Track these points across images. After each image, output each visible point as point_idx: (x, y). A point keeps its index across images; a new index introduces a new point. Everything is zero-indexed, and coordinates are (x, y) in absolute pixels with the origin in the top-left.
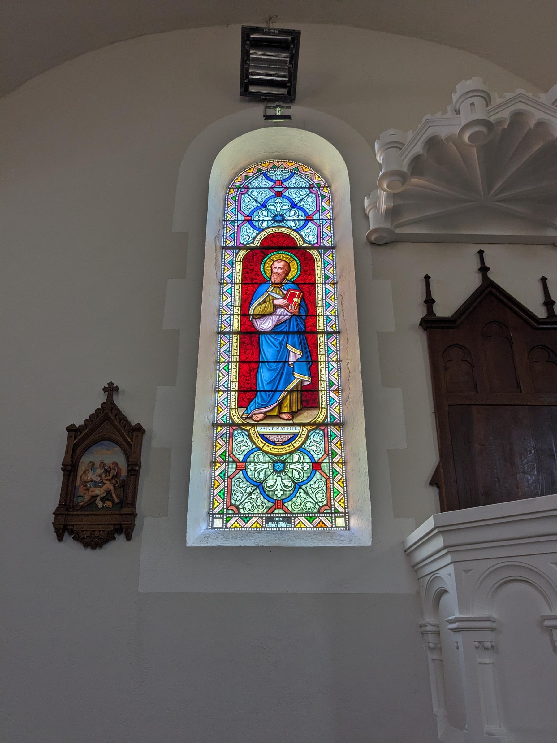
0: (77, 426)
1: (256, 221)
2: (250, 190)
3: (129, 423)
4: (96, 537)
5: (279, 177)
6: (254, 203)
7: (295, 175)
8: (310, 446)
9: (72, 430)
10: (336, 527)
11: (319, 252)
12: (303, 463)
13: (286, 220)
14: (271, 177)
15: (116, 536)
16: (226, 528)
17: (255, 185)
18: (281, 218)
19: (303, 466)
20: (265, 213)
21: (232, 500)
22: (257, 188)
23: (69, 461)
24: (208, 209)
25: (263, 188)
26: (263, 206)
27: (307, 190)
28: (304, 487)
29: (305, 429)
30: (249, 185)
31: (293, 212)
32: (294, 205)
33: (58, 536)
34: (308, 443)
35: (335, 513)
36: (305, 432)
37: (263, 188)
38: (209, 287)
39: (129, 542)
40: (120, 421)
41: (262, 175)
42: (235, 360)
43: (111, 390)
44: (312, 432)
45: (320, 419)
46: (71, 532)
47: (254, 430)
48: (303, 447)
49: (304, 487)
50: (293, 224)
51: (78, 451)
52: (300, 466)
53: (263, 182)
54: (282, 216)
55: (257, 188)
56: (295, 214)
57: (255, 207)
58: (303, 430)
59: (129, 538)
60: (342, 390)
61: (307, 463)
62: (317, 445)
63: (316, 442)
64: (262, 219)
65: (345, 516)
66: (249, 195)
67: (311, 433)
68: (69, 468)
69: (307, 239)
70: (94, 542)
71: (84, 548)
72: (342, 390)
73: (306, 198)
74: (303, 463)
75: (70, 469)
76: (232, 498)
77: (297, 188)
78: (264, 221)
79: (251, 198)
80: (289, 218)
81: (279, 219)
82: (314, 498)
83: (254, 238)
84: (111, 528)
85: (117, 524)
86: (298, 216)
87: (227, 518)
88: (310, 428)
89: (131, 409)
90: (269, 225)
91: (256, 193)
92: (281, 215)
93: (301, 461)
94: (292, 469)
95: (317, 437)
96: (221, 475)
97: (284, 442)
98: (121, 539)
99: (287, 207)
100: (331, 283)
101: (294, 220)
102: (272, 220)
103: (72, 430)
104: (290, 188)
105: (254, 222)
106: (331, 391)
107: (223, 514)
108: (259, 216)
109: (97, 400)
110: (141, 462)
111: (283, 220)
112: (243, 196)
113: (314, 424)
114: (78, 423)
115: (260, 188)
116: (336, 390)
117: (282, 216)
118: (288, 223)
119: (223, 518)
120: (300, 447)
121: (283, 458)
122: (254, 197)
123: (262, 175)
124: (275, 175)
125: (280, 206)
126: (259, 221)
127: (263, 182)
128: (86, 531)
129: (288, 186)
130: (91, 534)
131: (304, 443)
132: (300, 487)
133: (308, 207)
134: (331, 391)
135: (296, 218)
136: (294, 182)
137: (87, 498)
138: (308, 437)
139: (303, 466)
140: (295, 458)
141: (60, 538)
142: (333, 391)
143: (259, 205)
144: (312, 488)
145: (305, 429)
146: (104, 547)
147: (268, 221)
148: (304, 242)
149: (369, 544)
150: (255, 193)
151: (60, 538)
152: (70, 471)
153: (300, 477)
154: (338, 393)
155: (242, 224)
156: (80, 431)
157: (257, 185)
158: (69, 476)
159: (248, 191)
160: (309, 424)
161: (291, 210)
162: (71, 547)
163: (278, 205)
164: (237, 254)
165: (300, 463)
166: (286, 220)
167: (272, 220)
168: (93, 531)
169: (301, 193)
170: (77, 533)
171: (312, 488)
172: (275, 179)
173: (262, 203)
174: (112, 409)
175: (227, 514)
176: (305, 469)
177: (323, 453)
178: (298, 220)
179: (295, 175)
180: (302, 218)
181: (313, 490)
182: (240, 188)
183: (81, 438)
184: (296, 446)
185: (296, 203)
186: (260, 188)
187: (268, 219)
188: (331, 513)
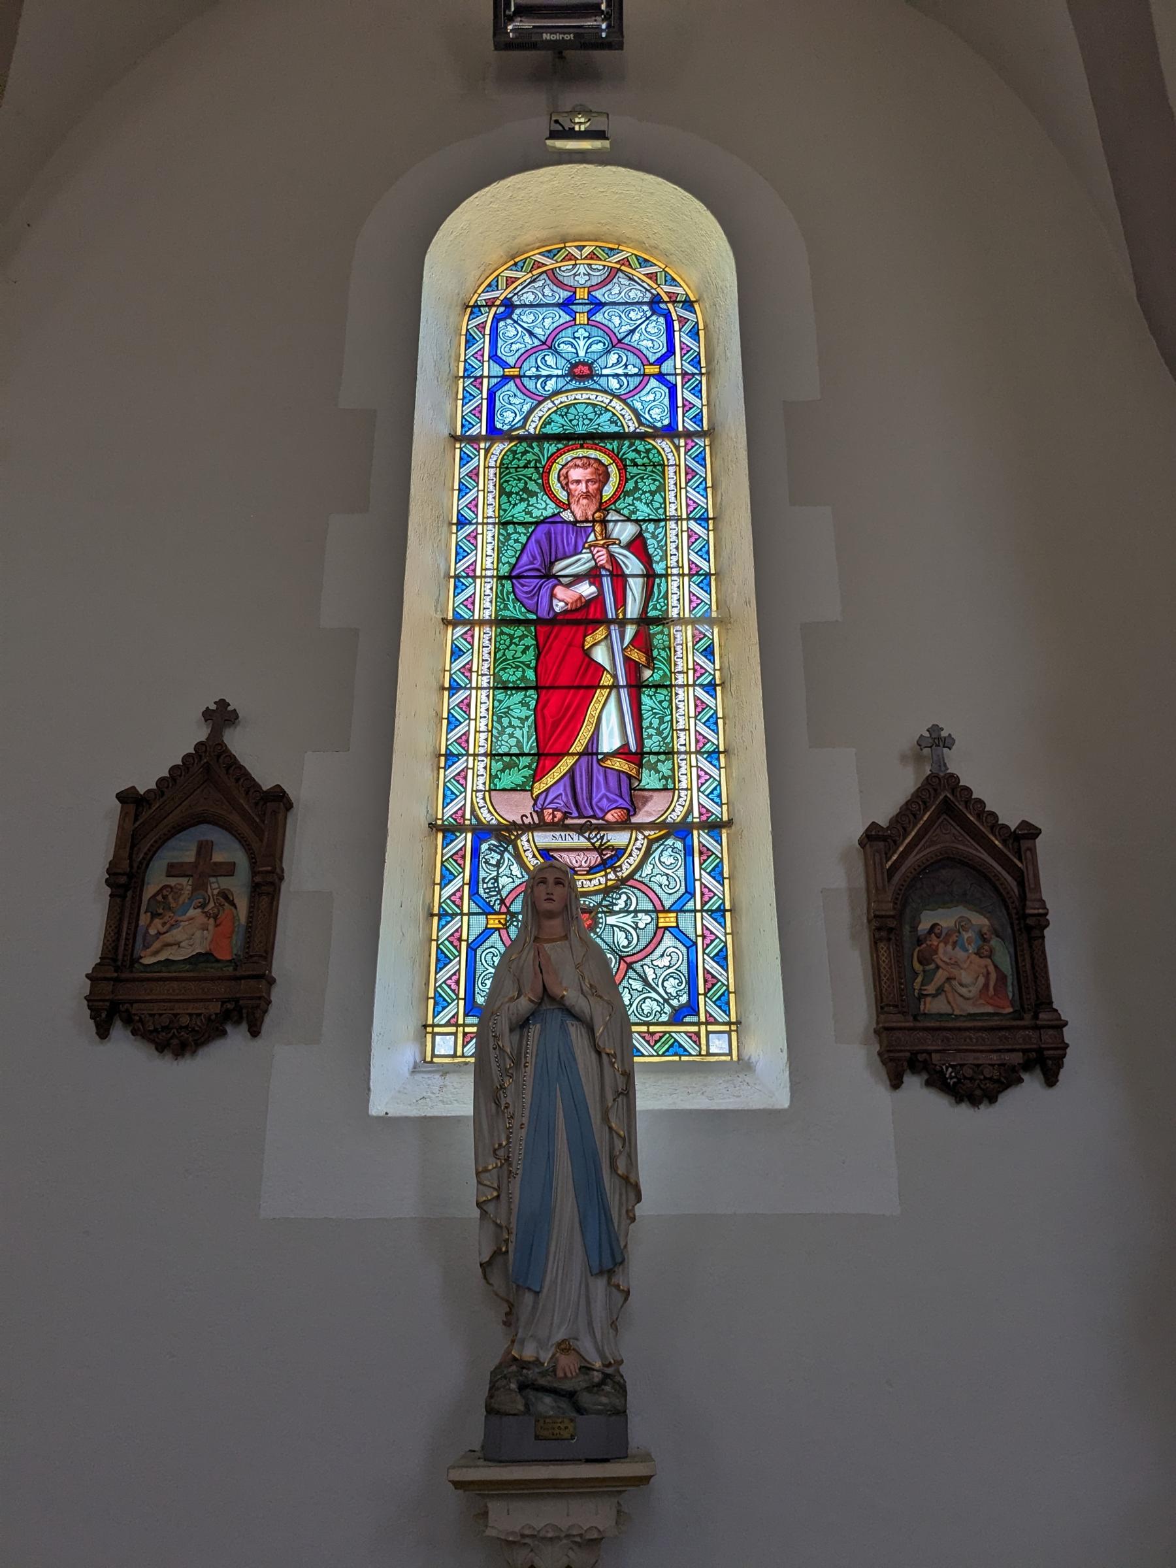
0: (142, 791)
1: (530, 377)
2: (518, 311)
3: (256, 786)
4: (181, 1028)
5: (582, 280)
6: (527, 338)
7: (620, 274)
8: (652, 875)
9: (127, 798)
10: (709, 1054)
11: (674, 444)
12: (636, 912)
13: (598, 375)
14: (565, 281)
15: (229, 1028)
16: (463, 1056)
17: (529, 298)
18: (586, 370)
19: (635, 920)
20: (550, 360)
21: (477, 996)
22: (531, 306)
23: (125, 866)
24: (412, 491)
25: (546, 305)
26: (549, 345)
27: (646, 308)
28: (637, 966)
29: (640, 836)
30: (515, 298)
31: (613, 358)
32: (616, 343)
33: (98, 1026)
34: (647, 870)
35: (707, 1023)
36: (642, 842)
37: (546, 305)
38: (424, 559)
39: (259, 1043)
40: (237, 780)
41: (544, 276)
42: (485, 685)
43: (221, 716)
44: (657, 845)
45: (677, 815)
46: (128, 1021)
47: (528, 841)
48: (637, 877)
49: (637, 966)
50: (614, 384)
51: (145, 846)
52: (629, 919)
53: (547, 291)
54: (590, 366)
55: (531, 306)
56: (618, 362)
57: (529, 347)
58: (637, 839)
59: (255, 1032)
60: (722, 684)
61: (646, 912)
62: (669, 872)
63: (667, 867)
64: (544, 373)
65: (729, 1033)
66: (516, 322)
67: (655, 846)
68: (123, 880)
69: (647, 416)
70: (177, 1038)
71: (156, 1053)
72: (722, 684)
73: (643, 326)
74: (636, 912)
75: (124, 882)
76: (477, 990)
77: (626, 303)
78: (550, 377)
79: (520, 329)
80: (605, 372)
81: (582, 372)
82: (661, 990)
83: (526, 418)
84: (215, 1008)
85: (229, 1001)
86: (626, 366)
87: (465, 1034)
88: (652, 834)
89: (258, 753)
90: (560, 386)
91: (532, 317)
92: (584, 363)
93: (632, 908)
94: (612, 926)
95: (669, 856)
96: (449, 982)
97: (591, 868)
98: (1032, 1084)
99: (600, 346)
100: (699, 518)
101: (617, 376)
102: (566, 375)
103: (127, 798)
104: (605, 304)
105: (526, 381)
106: (707, 911)
107: (457, 1025)
108: (538, 368)
109: (189, 735)
110: (282, 870)
111: (590, 376)
112: (501, 324)
113: (663, 825)
114: (145, 784)
115: (538, 305)
116: (718, 910)
117: (590, 366)
118: (602, 381)
119: (455, 1034)
120: (631, 876)
121: (575, 384)
122: (525, 325)
123: (544, 276)
124: (575, 275)
125: (581, 345)
126: (538, 377)
127: (547, 291)
128: (161, 1015)
129: (603, 300)
130: (171, 1022)
131: (640, 866)
132: (620, 341)
133: (664, 880)
134: (707, 911)
135: (620, 371)
136: (616, 290)
137: (173, 905)
138: (648, 853)
139: (635, 920)
140: (551, 385)
141: (103, 1032)
142: (701, 686)
143: (537, 343)
144: (654, 967)
145: (640, 836)
146: (203, 1052)
147: (557, 376)
148: (641, 424)
149: (786, 1104)
150: (527, 318)
151: (103, 1032)
152: (126, 887)
153: (630, 943)
154: (724, 916)
155: (499, 386)
156: (148, 801)
157: (531, 297)
158: (124, 897)
159: (512, 312)
160: (652, 825)
161: (609, 352)
162: (125, 1051)
163: (581, 343)
164: (487, 451)
165: (629, 912)
166: (598, 375)
167: (566, 375)
168: (175, 1015)
169: (632, 315)
170: (141, 1020)
171: (654, 967)
172: (575, 284)
173: (543, 338)
174: (219, 757)
175: (464, 1025)
176: (641, 925)
177: (683, 890)
178: (626, 375)
179: (620, 274)
180: (636, 371)
181: (658, 971)
182: (493, 305)
183: (146, 818)
184: (626, 871)
185: (620, 336)
186: (538, 305)
187: (559, 372)
188: (698, 1024)
